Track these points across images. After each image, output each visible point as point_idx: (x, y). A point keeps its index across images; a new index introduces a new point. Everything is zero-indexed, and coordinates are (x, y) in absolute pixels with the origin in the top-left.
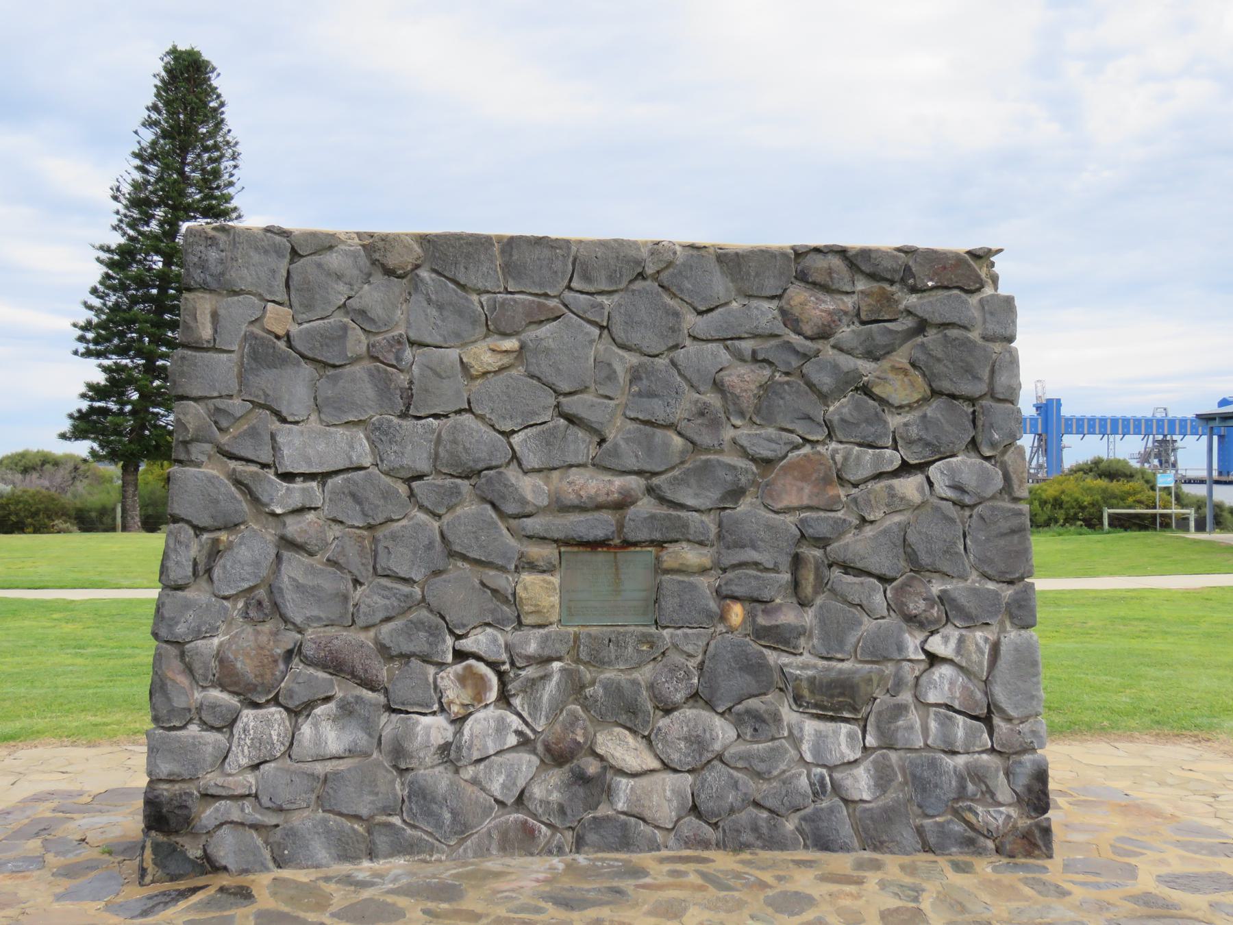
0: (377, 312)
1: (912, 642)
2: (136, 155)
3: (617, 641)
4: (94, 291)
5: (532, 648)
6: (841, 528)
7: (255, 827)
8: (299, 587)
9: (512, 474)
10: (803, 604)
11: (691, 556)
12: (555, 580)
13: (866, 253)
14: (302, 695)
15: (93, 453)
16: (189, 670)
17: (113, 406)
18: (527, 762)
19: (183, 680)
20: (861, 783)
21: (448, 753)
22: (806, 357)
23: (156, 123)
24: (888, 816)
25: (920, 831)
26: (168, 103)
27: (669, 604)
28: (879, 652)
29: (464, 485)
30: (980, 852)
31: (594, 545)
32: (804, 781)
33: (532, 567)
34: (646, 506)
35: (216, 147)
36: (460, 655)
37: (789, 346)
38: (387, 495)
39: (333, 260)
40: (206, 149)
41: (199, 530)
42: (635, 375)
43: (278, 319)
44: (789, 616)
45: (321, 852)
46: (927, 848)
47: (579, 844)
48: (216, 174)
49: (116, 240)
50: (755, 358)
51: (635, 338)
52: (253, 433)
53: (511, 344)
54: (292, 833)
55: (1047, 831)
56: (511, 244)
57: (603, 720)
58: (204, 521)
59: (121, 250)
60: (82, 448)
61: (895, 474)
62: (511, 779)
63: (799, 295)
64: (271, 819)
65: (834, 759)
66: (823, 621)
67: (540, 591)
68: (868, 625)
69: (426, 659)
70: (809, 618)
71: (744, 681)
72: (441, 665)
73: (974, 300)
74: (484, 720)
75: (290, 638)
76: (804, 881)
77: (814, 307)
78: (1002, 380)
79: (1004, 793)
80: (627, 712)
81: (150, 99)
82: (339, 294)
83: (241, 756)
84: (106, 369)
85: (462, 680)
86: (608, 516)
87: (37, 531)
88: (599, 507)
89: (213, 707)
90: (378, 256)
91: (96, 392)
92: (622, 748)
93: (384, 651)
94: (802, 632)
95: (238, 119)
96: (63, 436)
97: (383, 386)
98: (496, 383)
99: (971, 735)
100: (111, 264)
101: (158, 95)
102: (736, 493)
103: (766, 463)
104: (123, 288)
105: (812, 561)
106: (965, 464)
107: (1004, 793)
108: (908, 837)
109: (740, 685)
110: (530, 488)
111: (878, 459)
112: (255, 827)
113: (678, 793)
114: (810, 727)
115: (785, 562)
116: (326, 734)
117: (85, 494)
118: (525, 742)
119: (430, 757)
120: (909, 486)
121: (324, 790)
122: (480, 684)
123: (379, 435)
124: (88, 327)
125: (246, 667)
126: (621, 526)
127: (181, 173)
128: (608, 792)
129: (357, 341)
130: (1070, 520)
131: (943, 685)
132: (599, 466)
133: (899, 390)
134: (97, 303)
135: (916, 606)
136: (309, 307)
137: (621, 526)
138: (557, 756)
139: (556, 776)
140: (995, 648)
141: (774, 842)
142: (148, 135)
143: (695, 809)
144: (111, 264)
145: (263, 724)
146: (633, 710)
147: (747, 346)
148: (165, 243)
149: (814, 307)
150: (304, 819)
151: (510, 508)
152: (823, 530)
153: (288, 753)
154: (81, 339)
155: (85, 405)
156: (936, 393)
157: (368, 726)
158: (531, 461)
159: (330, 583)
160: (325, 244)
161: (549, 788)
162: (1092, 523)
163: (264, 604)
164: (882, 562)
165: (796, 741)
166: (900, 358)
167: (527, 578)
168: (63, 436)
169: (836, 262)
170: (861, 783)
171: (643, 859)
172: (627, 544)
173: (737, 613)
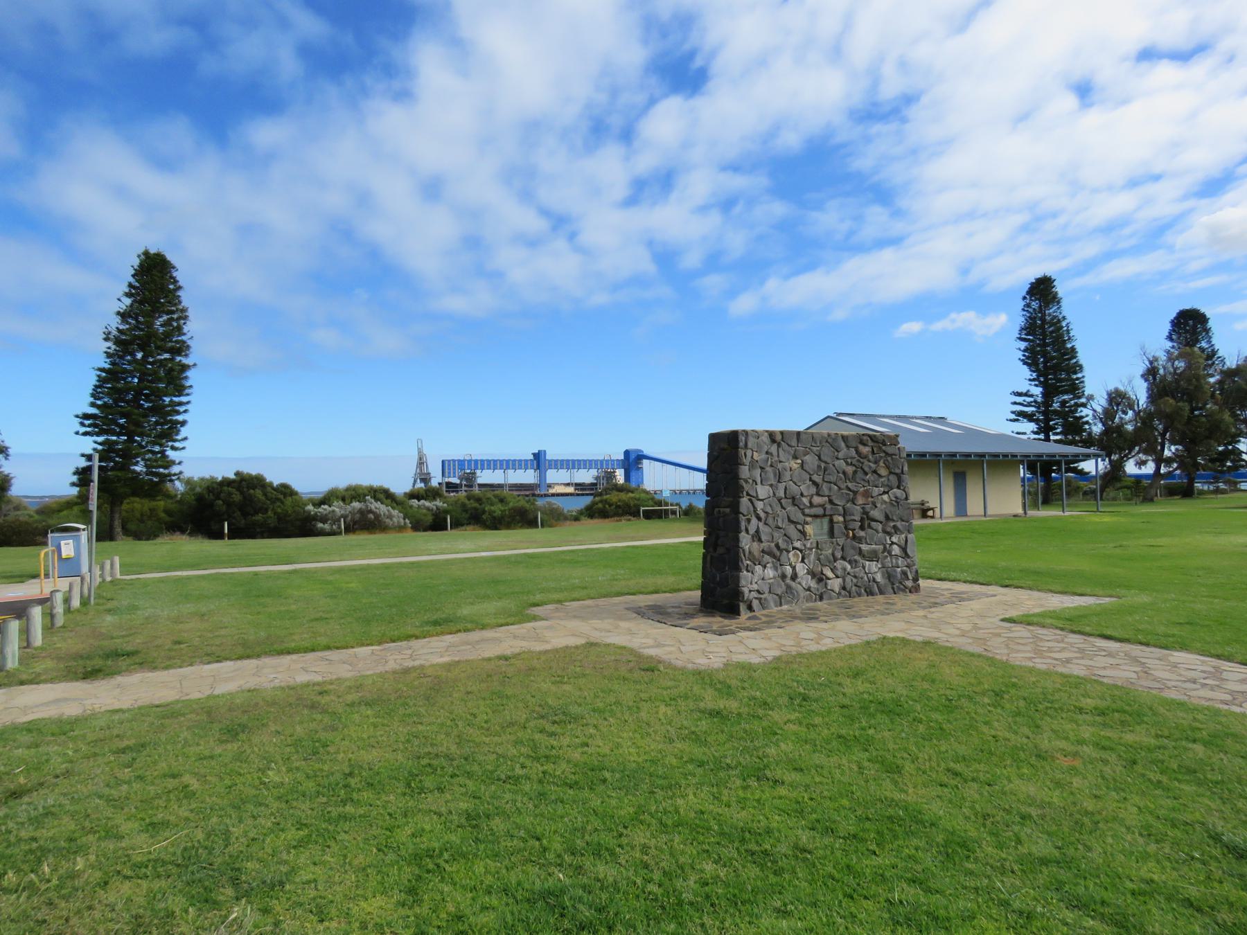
105: (866, 520)
120: (885, 497)
135: (889, 529)
142: (128, 301)
165: (864, 567)
170: (879, 578)
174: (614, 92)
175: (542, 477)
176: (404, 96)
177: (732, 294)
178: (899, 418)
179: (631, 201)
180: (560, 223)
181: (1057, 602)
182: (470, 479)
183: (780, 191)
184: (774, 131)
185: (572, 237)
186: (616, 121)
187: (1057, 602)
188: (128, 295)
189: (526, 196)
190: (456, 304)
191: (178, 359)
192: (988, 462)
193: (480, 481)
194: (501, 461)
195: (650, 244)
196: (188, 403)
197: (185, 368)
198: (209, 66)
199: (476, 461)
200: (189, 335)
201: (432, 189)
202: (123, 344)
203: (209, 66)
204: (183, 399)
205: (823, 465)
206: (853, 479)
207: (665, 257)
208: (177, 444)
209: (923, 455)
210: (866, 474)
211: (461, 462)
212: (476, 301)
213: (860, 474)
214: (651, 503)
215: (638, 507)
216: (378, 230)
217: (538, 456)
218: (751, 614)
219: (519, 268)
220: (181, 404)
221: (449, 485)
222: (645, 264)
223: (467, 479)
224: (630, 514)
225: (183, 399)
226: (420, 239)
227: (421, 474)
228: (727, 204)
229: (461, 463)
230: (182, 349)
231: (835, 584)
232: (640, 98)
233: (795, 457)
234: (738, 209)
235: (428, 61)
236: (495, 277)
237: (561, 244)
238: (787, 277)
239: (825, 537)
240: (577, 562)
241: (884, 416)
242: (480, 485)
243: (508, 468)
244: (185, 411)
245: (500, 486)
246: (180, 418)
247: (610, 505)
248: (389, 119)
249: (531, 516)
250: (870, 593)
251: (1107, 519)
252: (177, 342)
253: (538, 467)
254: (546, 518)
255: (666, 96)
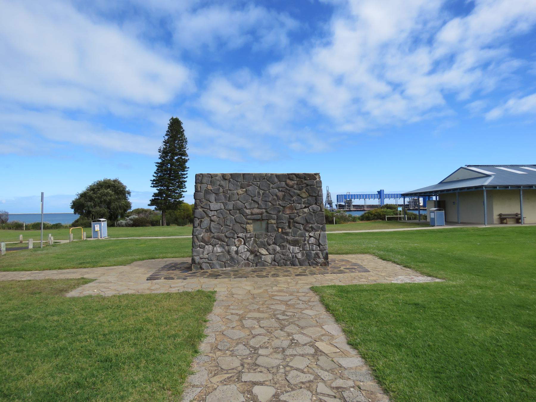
0: (224, 185)
1: (307, 234)
2: (164, 142)
3: (262, 235)
4: (155, 173)
5: (249, 236)
6: (296, 216)
7: (208, 263)
8: (213, 227)
9: (245, 210)
10: (290, 228)
11: (273, 221)
12: (252, 225)
13: (298, 174)
14: (214, 243)
15: (155, 208)
16: (198, 240)
17: (160, 198)
18: (249, 253)
19: (197, 241)
20: (299, 256)
21: (237, 252)
22: (289, 190)
23: (169, 135)
24: (304, 260)
25: (309, 263)
26: (171, 130)
27: (269, 229)
28: (302, 235)
29: (238, 211)
30: (318, 266)
31: (258, 220)
32: (291, 256)
33: (249, 224)
34: (265, 214)
35: (182, 140)
36: (238, 237)
37: (287, 189)
38: (226, 213)
39: (217, 178)
40: (179, 140)
41: (199, 219)
42: (263, 194)
43: (210, 187)
44: (288, 230)
45: (218, 266)
46: (310, 265)
47: (256, 266)
48: (182, 146)
49: (160, 161)
50: (282, 191)
51: (263, 188)
52: (206, 204)
53: (244, 190)
54: (213, 264)
55: (328, 262)
56: (244, 175)
57: (259, 247)
58: (199, 217)
59: (160, 163)
60: (153, 208)
61: (304, 208)
62: (246, 256)
63: (288, 181)
64: (210, 262)
65: (295, 252)
66: (293, 231)
67: (250, 227)
68: (300, 231)
69: (233, 238)
70: (291, 231)
71: (281, 240)
72: (235, 239)
73: (315, 181)
74: (241, 247)
75: (212, 235)
76: (289, 269)
77: (291, 183)
78: (320, 193)
79: (321, 256)
80: (264, 245)
81: (167, 129)
82: (218, 183)
83: (206, 253)
84: (157, 190)
85: (238, 241)
86: (260, 216)
87: (142, 226)
88: (258, 214)
89: (202, 245)
90: (224, 176)
91: (155, 195)
92: (263, 251)
93: (226, 237)
94: (289, 233)
95: (188, 134)
96: (149, 205)
97: (225, 197)
98: (242, 196)
99: (316, 248)
100: (158, 167)
101: (169, 128)
102: (279, 212)
103: (284, 207)
104: (161, 171)
105: (292, 222)
106: (314, 206)
107: (321, 256)
108: (307, 264)
109: (281, 241)
110: (248, 211)
111: (301, 206)
112: (208, 263)
113: (272, 258)
114: (291, 247)
115: (287, 222)
116: (218, 249)
117: (152, 218)
118: (248, 250)
119: (234, 253)
120: (306, 210)
121: (218, 258)
122: (241, 241)
123: (225, 204)
124: (154, 180)
125: (206, 239)
126: (262, 217)
127: (174, 146)
128: (261, 258)
129: (221, 190)
130: (378, 219)
131: (312, 240)
132: (258, 208)
133: (304, 195)
134: (156, 175)
135: (307, 228)
136: (214, 185)
137: (262, 217)
138: (252, 252)
139: (253, 256)
140: (320, 234)
141: (286, 265)
142: (167, 138)
143: (274, 261)
144: (158, 167)
145: (209, 248)
146: (265, 245)
147: (281, 189)
148: (171, 161)
149: (291, 183)
150: (215, 262)
151: (245, 215)
152: (293, 217)
153: (212, 252)
154: (152, 183)
155: (153, 198)
156: (310, 196)
157: (224, 248)
158: (248, 207)
159: (217, 226)
160: (216, 175)
161: (251, 257)
162: (383, 219)
163: (209, 230)
164: (302, 222)
165: (289, 249)
166: (304, 190)
167: (248, 225)
168: (149, 205)
169: (294, 176)
170: (299, 256)
171: (267, 268)
172: (263, 220)
173: (280, 230)
174: (425, 23)
175: (382, 201)
176: (328, 44)
177: (487, 109)
178: (512, 166)
179: (432, 72)
180: (397, 87)
182: (349, 203)
183: (516, 54)
184: (515, 22)
185: (402, 92)
186: (425, 36)
188: (167, 135)
189: (381, 77)
190: (348, 128)
191: (183, 157)
192: (523, 191)
193: (353, 204)
194: (363, 195)
195: (442, 90)
197: (186, 161)
198: (256, 47)
199: (352, 195)
201: (339, 81)
202: (164, 153)
203: (256, 47)
204: (185, 173)
206: (283, 199)
207: (450, 96)
208: (184, 190)
209: (507, 187)
210: (292, 197)
211: (345, 196)
212: (359, 125)
213: (287, 197)
214: (392, 213)
215: (385, 215)
216: (316, 101)
217: (380, 193)
218: (203, 271)
219: (375, 108)
220: (184, 174)
221: (340, 206)
222: (440, 100)
223: (348, 203)
224: (381, 219)
225: (185, 173)
226: (333, 102)
227: (328, 201)
228: (485, 66)
232: (439, 23)
234: (491, 67)
235: (339, 29)
236: (366, 114)
237: (397, 96)
238: (521, 97)
241: (525, 166)
242: (354, 206)
245: (363, 206)
246: (185, 180)
247: (371, 214)
248: (322, 55)
249: (331, 219)
250: (293, 264)
253: (380, 198)
255: (451, 19)
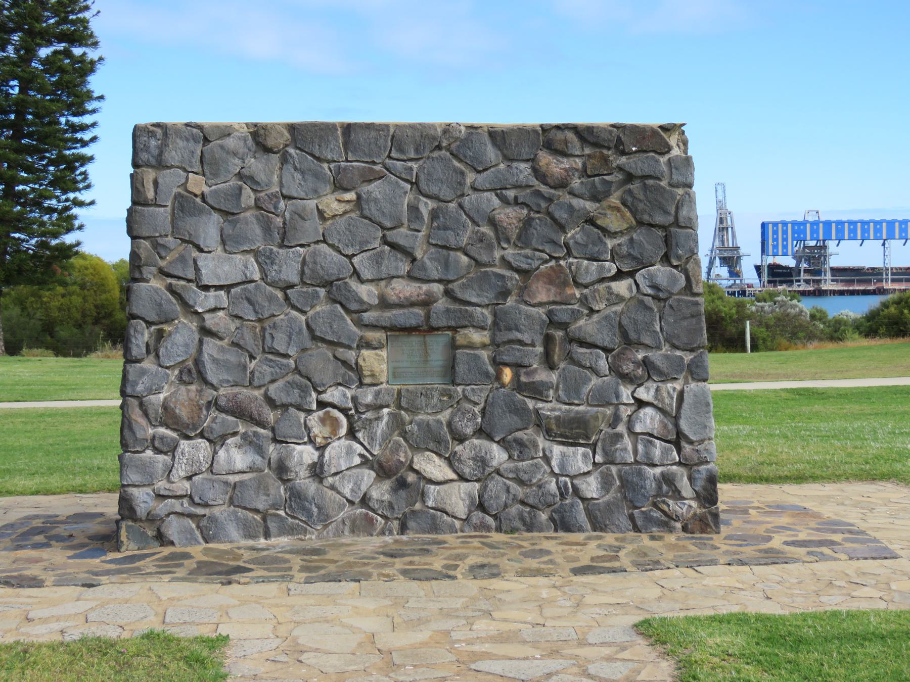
105: (560, 339)
120: (622, 287)
135: (628, 367)
165: (547, 459)
170: (591, 487)
181: (279, 574)
187: (279, 574)
191: (77, 51)
196: (94, 125)
199: (828, 224)
200: (94, 9)
204: (87, 119)
205: (426, 206)
206: (523, 240)
210: (562, 228)
213: (541, 228)
218: (167, 551)
220: (83, 128)
223: (808, 260)
225: (87, 119)
227: (723, 249)
229: (798, 227)
230: (81, 35)
231: (458, 498)
233: (339, 186)
239: (437, 383)
240: (96, 414)
242: (836, 271)
243: (891, 236)
244: (94, 139)
249: (732, 330)
251: (557, 349)
252: (73, 22)
254: (763, 332)
